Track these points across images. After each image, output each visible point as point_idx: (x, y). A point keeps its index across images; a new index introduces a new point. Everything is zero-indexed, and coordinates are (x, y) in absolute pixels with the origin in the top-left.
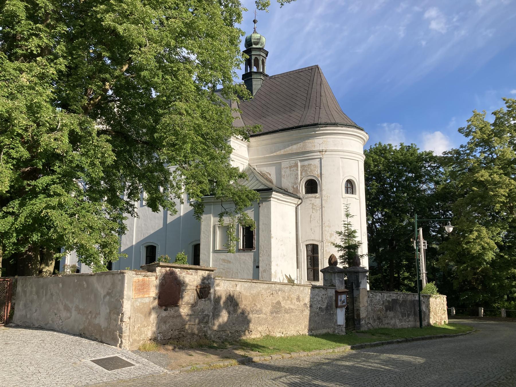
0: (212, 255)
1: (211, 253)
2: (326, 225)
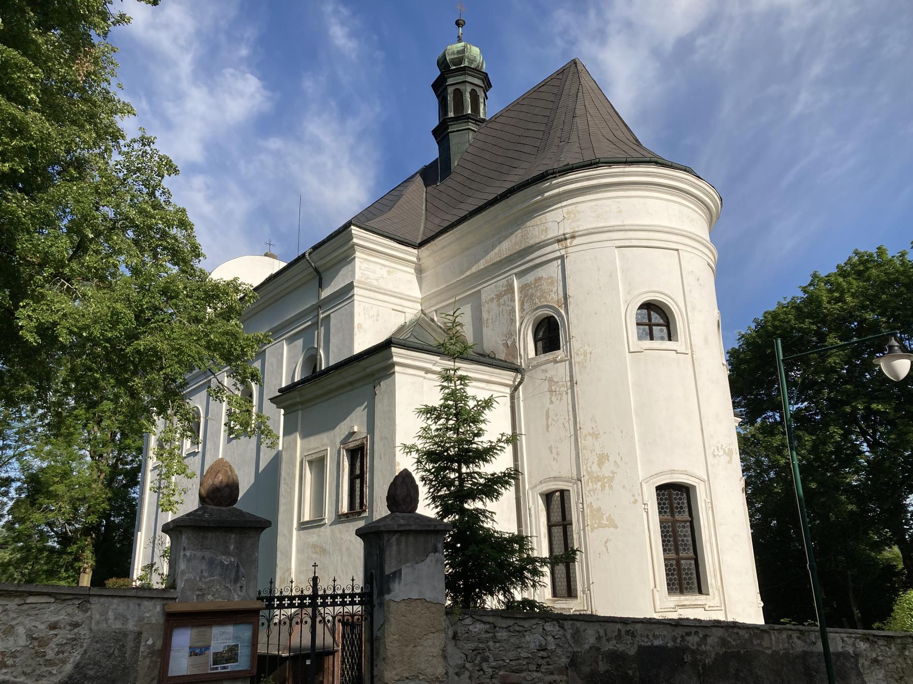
0: (298, 536)
1: (295, 532)
2: (584, 431)
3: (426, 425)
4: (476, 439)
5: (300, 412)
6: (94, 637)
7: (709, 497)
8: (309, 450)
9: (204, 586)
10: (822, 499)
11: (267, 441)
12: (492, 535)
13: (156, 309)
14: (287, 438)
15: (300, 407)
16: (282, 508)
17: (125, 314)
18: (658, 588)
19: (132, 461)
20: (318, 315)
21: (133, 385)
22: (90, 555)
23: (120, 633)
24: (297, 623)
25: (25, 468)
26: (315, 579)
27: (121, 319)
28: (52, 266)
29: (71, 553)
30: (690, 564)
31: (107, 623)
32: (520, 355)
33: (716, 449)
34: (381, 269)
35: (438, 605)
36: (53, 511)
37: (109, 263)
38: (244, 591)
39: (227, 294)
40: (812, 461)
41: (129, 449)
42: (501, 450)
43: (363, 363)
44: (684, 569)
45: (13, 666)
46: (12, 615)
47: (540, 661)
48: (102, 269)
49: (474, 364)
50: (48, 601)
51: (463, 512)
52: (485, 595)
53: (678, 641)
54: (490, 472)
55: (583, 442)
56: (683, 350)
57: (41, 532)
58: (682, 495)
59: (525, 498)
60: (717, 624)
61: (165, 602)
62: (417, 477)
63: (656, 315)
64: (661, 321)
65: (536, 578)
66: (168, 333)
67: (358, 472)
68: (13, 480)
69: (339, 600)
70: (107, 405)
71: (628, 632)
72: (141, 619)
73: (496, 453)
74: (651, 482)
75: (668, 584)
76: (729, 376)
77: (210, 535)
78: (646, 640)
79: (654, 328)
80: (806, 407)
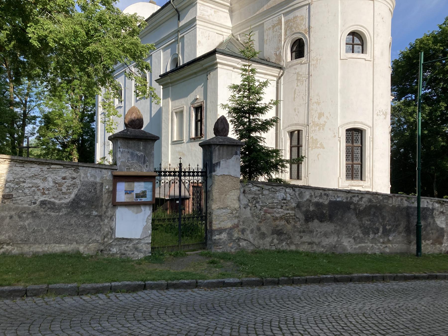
1: (170, 146)
2: (313, 101)
3: (233, 94)
4: (258, 102)
5: (170, 88)
6: (82, 184)
7: (372, 136)
8: (175, 107)
9: (129, 165)
10: (429, 139)
11: (155, 101)
12: (263, 149)
13: (96, 30)
14: (164, 100)
15: (170, 85)
16: (163, 131)
17: (81, 32)
18: (341, 177)
19: (91, 110)
20: (178, 36)
21: (88, 71)
22: (76, 153)
23: (93, 183)
24: (173, 183)
25: (42, 111)
26: (180, 164)
27: (79, 35)
28: (40, 4)
29: (67, 152)
30: (358, 167)
31: (87, 178)
32: (283, 60)
33: (379, 111)
34: (211, 10)
35: (237, 178)
36: (57, 132)
37: (69, 3)
38: (148, 168)
39: (132, 22)
40: (427, 120)
41: (89, 104)
42: (270, 108)
43: (201, 62)
44: (355, 169)
45: (49, 194)
46: (45, 173)
47: (283, 205)
48: (66, 6)
49: (259, 64)
50: (61, 167)
51: (250, 137)
52: (259, 175)
53: (349, 199)
54: (264, 119)
55: (312, 106)
56: (368, 58)
57: (53, 141)
58: (358, 134)
59: (280, 134)
60: (368, 193)
61: (112, 171)
62: (229, 120)
63: (357, 39)
64: (359, 43)
65: (283, 169)
66: (103, 43)
67: (199, 118)
68: (37, 117)
69: (191, 174)
70: (76, 82)
71: (325, 194)
72: (102, 177)
73: (268, 110)
74: (344, 127)
75: (346, 176)
76: (391, 74)
77: (131, 142)
78: (333, 198)
79: (355, 46)
80: (429, 92)
